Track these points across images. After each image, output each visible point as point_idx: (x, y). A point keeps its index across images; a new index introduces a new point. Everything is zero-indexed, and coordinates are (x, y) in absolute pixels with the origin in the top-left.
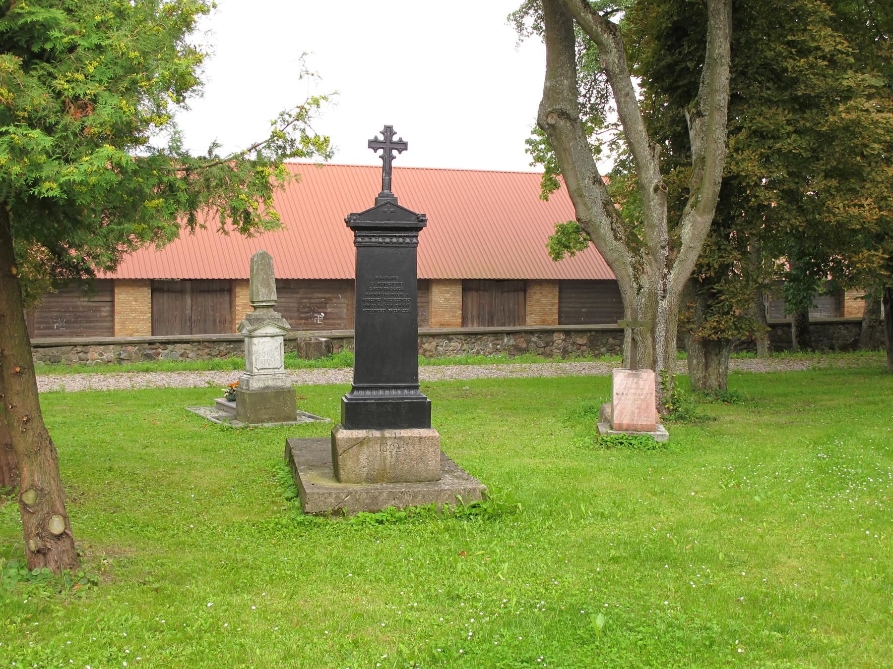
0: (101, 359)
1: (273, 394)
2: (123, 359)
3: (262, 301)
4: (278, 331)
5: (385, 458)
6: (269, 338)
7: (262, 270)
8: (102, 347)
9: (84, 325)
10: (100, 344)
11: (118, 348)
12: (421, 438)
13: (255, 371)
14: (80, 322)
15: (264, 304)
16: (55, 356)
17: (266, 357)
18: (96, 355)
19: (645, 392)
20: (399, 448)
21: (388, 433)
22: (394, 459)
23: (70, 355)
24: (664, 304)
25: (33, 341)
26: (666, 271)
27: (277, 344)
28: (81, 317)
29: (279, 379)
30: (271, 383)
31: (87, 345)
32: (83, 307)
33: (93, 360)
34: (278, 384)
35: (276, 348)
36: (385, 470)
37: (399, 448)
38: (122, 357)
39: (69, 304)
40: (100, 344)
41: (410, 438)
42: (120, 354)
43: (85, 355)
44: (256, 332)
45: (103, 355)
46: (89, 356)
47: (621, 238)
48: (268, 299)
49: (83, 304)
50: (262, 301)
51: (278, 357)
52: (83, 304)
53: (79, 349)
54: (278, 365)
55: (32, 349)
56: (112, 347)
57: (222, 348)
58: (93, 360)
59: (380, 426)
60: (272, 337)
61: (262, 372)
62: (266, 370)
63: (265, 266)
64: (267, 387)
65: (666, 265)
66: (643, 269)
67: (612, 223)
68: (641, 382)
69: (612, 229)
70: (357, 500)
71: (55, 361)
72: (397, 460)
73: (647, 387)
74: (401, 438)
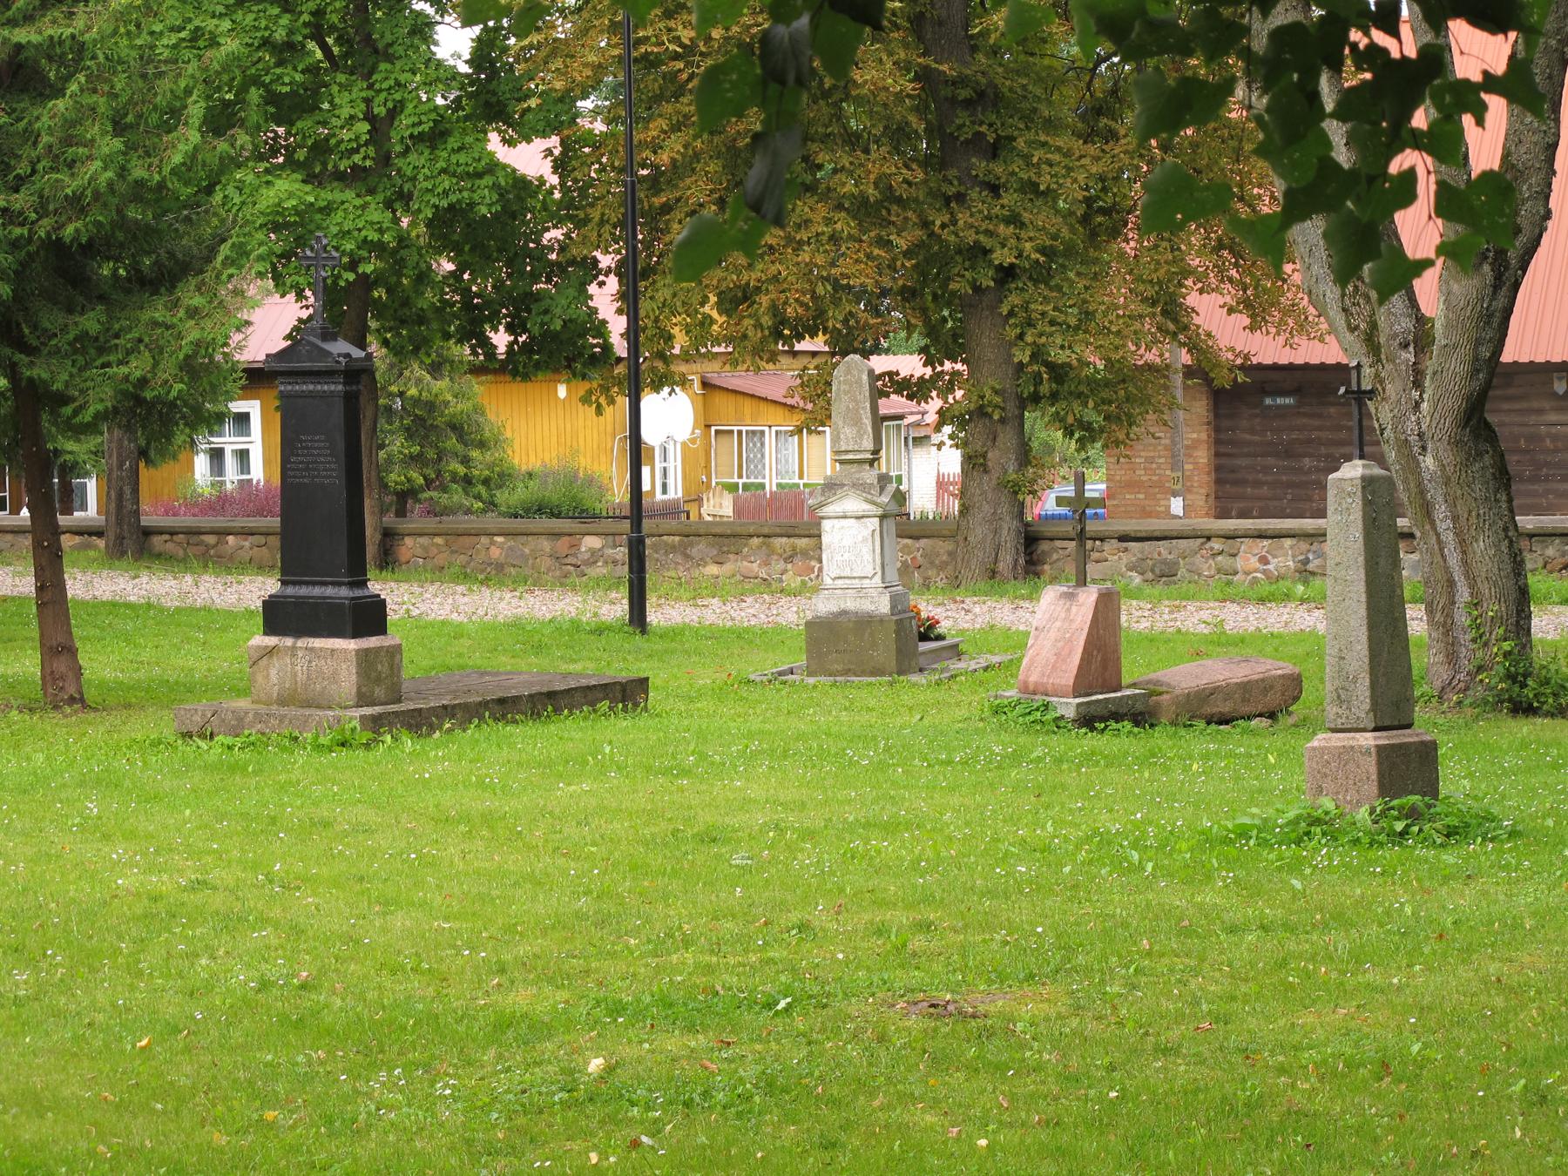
0: (1264, 572)
1: (851, 625)
2: (1313, 573)
3: (847, 452)
4: (862, 507)
5: (295, 675)
6: (853, 520)
7: (846, 393)
8: (1266, 543)
9: (1556, 486)
10: (1261, 535)
11: (1304, 546)
12: (333, 650)
13: (827, 581)
14: (1546, 480)
15: (851, 457)
16: (1164, 562)
17: (846, 556)
18: (1254, 562)
19: (1074, 626)
20: (310, 662)
21: (301, 643)
22: (305, 676)
23: (1198, 559)
24: (1429, 462)
25: (1527, 522)
26: (1415, 394)
27: (867, 533)
28: (1547, 464)
29: (866, 597)
30: (851, 605)
31: (1234, 538)
32: (1555, 438)
33: (1247, 574)
34: (864, 607)
35: (865, 540)
36: (296, 690)
37: (310, 662)
38: (1310, 567)
39: (1516, 430)
40: (1261, 535)
41: (321, 649)
42: (1306, 561)
43: (1231, 560)
44: (826, 509)
45: (1267, 562)
46: (1239, 563)
47: (1357, 328)
48: (856, 448)
49: (1553, 430)
50: (847, 452)
51: (868, 557)
52: (1553, 430)
53: (1216, 545)
54: (869, 571)
55: (1524, 544)
56: (1288, 542)
57: (1550, 552)
58: (1247, 574)
59: (299, 633)
60: (858, 518)
61: (839, 583)
62: (847, 581)
63: (851, 386)
64: (844, 612)
65: (1414, 382)
66: (1384, 390)
67: (1343, 295)
68: (1074, 609)
69: (1344, 310)
70: (223, 721)
71: (1165, 574)
72: (309, 678)
73: (1079, 619)
74: (312, 649)
